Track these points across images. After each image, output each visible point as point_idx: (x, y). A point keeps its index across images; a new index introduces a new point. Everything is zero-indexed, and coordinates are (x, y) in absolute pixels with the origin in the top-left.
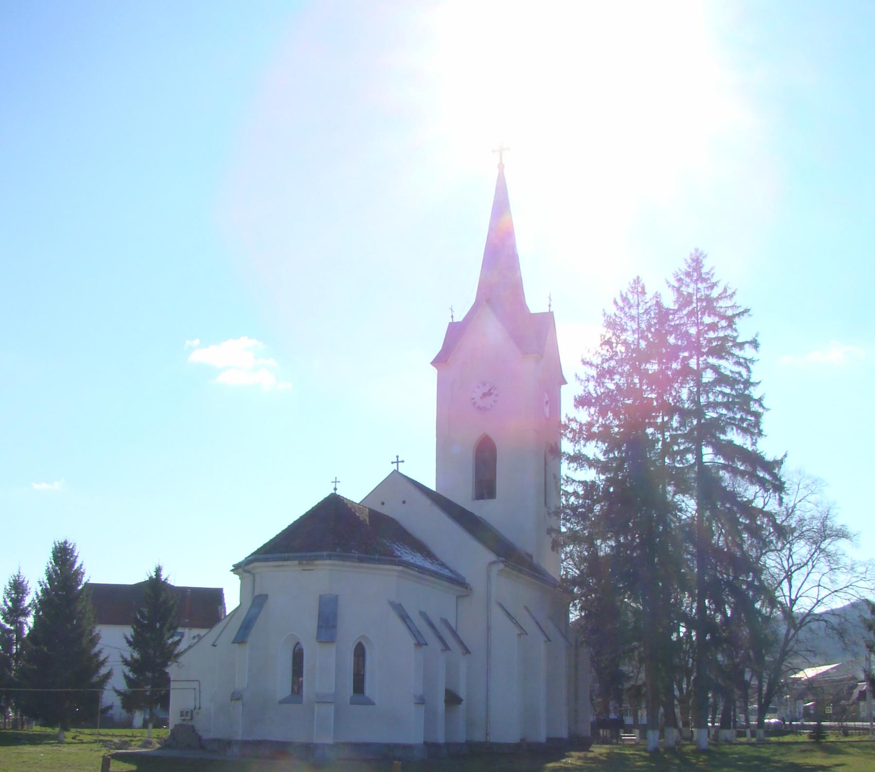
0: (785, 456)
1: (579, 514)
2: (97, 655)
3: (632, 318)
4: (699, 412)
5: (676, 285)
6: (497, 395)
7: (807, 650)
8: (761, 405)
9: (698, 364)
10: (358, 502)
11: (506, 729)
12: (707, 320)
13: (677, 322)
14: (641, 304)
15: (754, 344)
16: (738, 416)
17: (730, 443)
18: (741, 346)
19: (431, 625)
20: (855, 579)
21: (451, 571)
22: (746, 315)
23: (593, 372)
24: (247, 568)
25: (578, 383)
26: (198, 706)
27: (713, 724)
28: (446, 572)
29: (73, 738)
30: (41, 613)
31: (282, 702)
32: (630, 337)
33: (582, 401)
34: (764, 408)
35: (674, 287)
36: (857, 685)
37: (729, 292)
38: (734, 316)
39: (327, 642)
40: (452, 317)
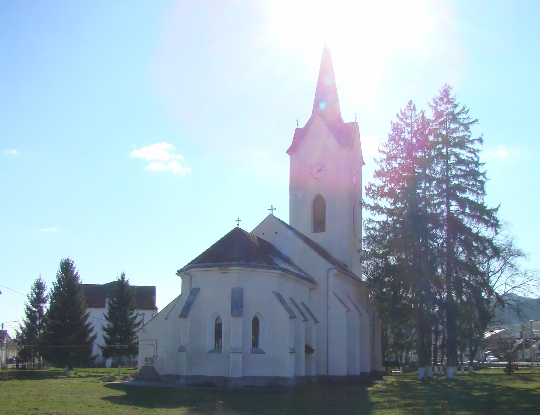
0: (499, 206)
1: (372, 239)
2: (88, 325)
3: (407, 125)
4: (446, 180)
5: (434, 105)
6: (326, 171)
7: (499, 321)
8: (484, 177)
9: (447, 152)
10: (249, 232)
11: (339, 367)
12: (453, 126)
13: (435, 127)
14: (413, 116)
15: (480, 140)
16: (471, 183)
17: (467, 199)
18: (472, 142)
19: (296, 306)
20: (527, 280)
21: (305, 274)
22: (476, 123)
23: (385, 157)
24: (187, 272)
25: (376, 163)
26: (156, 355)
27: (442, 363)
28: (303, 274)
29: (75, 374)
30: (54, 301)
31: (209, 353)
32: (407, 136)
33: (378, 174)
34: (486, 178)
35: (433, 106)
36: (516, 341)
37: (466, 110)
38: (469, 124)
39: (238, 316)
40: (298, 125)
